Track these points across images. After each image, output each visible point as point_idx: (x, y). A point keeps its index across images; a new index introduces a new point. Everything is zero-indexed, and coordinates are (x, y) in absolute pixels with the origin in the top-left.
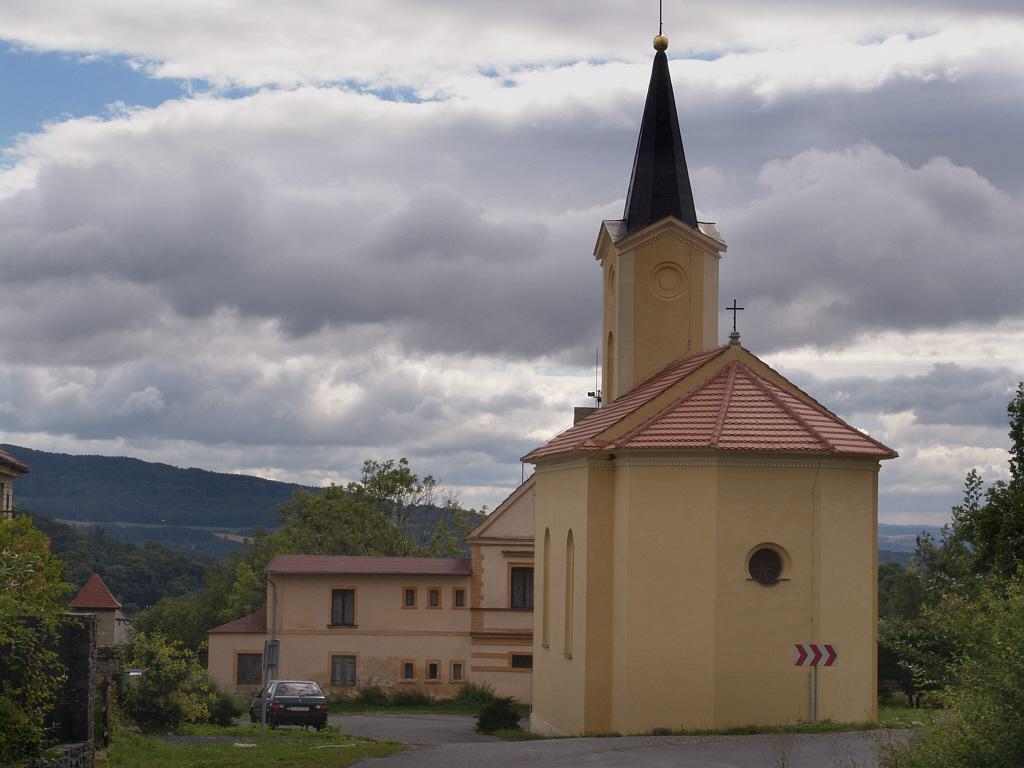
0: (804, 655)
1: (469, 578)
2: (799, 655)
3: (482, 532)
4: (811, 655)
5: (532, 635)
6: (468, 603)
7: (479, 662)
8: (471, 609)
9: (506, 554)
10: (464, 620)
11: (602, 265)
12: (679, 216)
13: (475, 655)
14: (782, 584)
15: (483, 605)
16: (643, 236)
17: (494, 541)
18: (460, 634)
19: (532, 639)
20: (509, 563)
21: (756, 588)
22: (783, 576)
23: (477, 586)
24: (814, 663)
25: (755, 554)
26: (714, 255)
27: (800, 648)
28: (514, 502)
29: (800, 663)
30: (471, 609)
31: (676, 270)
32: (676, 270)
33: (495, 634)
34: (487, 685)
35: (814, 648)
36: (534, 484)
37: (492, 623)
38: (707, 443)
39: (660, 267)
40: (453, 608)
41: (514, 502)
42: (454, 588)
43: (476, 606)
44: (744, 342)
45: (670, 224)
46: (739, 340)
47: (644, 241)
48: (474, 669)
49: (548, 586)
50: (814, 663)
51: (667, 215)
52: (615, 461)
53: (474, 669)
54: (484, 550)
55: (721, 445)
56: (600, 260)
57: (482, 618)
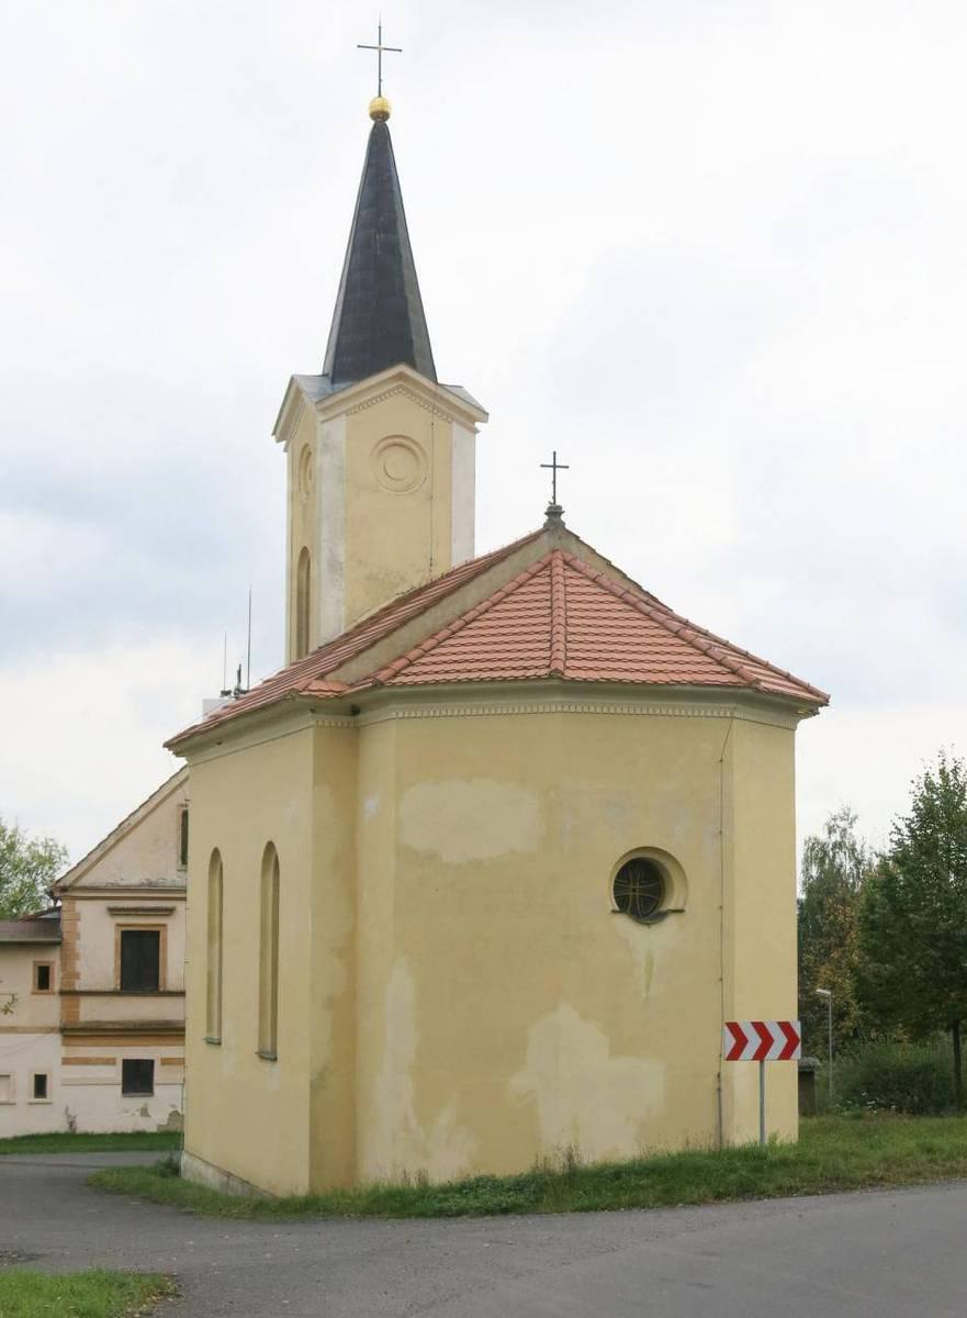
0: (741, 1042)
1: (58, 948)
2: (730, 1041)
3: (78, 879)
4: (754, 1040)
5: (183, 1029)
6: (56, 984)
7: (76, 1072)
8: (62, 993)
9: (113, 911)
10: (50, 1008)
11: (285, 450)
12: (413, 365)
13: (66, 1061)
14: (671, 920)
15: (79, 986)
16: (359, 394)
17: (95, 893)
18: (51, 1030)
19: (184, 1036)
20: (118, 925)
21: (625, 924)
22: (670, 904)
23: (69, 957)
24: (760, 1055)
25: (619, 876)
26: (466, 427)
27: (734, 1028)
28: (158, 805)
29: (735, 1055)
30: (62, 993)
31: (409, 449)
32: (409, 449)
33: (115, 1030)
34: (541, 1161)
35: (760, 1027)
36: (187, 779)
37: (90, 1011)
38: (545, 671)
39: (390, 441)
40: (33, 993)
41: (158, 805)
42: (35, 963)
43: (67, 989)
44: (570, 521)
45: (401, 376)
46: (563, 518)
47: (374, 395)
48: (66, 1084)
49: (180, 957)
50: (760, 1055)
51: (392, 363)
52: (361, 716)
53: (66, 1084)
54: (80, 906)
55: (570, 674)
56: (284, 443)
57: (77, 1006)
